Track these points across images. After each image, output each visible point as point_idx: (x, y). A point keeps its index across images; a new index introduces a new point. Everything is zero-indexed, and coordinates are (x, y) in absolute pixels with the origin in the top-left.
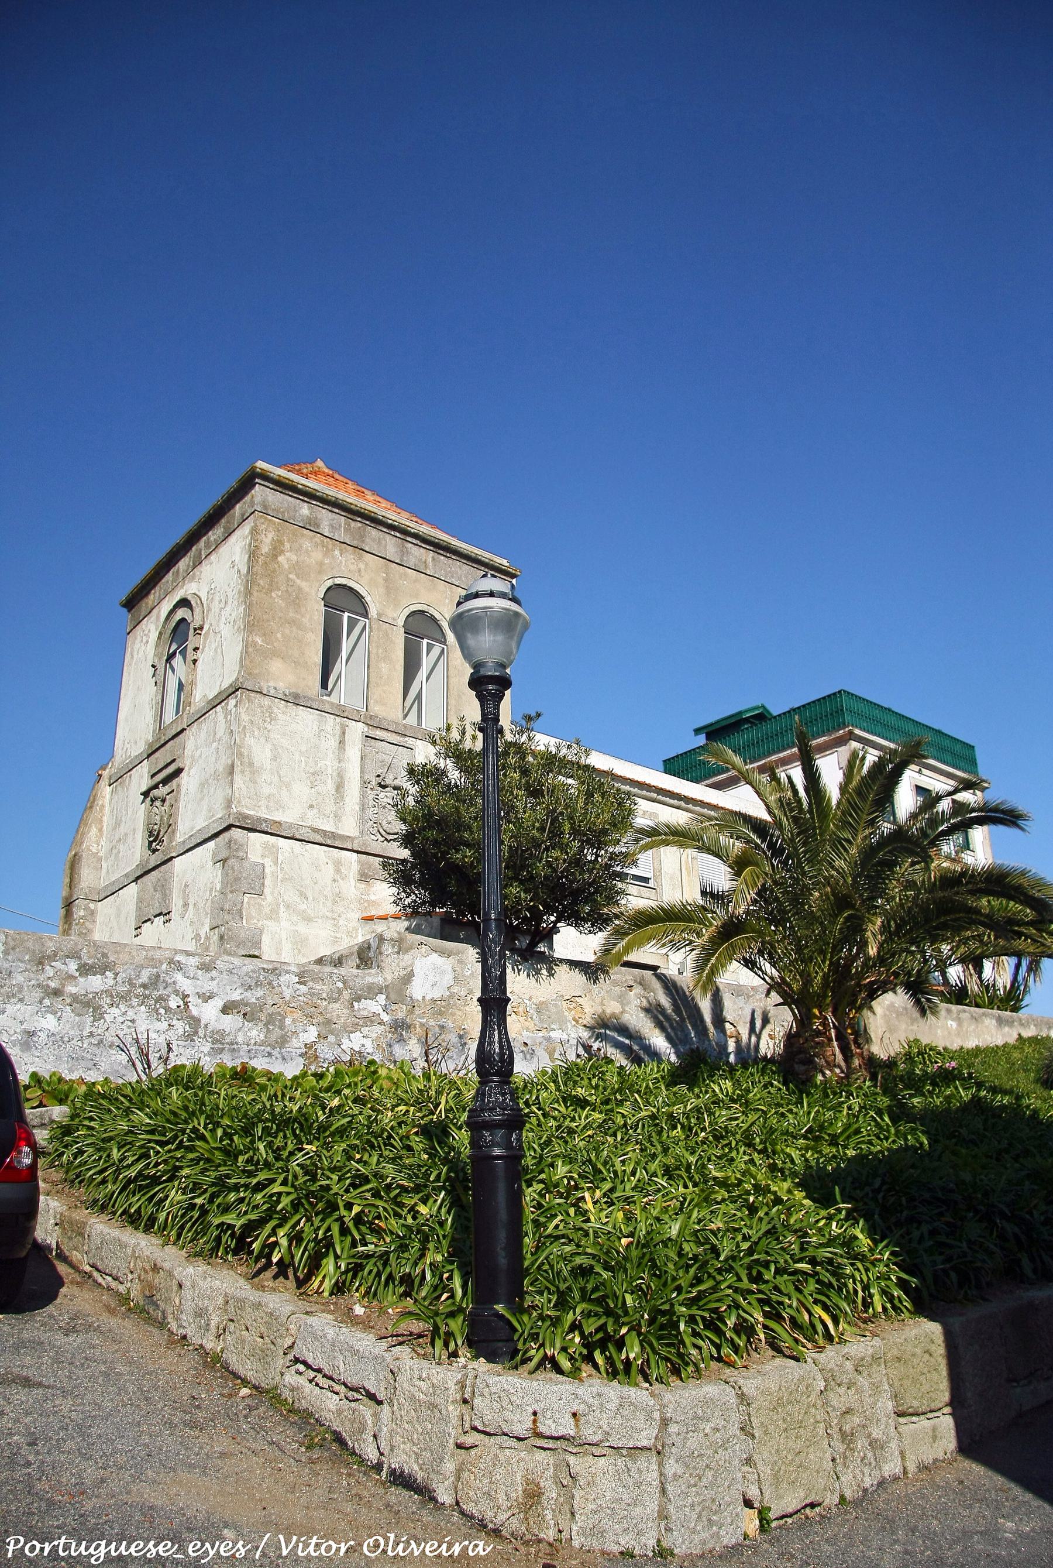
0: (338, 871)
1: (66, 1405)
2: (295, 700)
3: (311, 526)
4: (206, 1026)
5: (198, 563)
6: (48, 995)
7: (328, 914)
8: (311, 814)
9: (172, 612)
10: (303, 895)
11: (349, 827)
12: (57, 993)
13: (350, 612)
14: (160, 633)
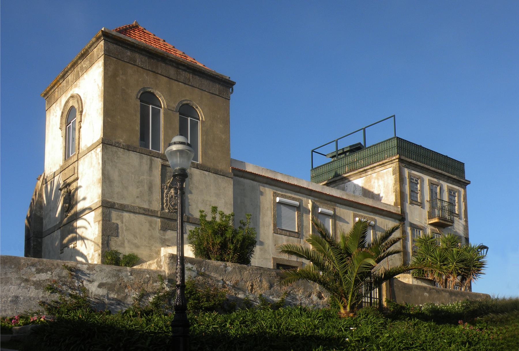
0: (151, 226)
1: (363, 322)
2: (128, 148)
3: (132, 62)
4: (92, 293)
5: (78, 77)
6: (23, 281)
7: (147, 245)
8: (137, 201)
9: (67, 102)
10: (135, 236)
11: (156, 206)
12: (27, 280)
13: (152, 105)
14: (63, 113)
